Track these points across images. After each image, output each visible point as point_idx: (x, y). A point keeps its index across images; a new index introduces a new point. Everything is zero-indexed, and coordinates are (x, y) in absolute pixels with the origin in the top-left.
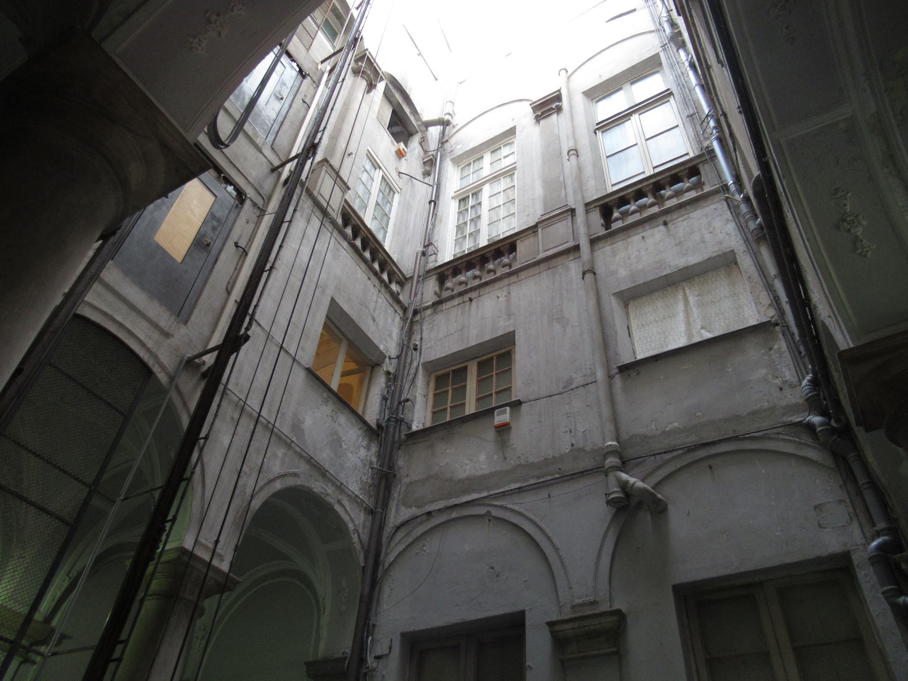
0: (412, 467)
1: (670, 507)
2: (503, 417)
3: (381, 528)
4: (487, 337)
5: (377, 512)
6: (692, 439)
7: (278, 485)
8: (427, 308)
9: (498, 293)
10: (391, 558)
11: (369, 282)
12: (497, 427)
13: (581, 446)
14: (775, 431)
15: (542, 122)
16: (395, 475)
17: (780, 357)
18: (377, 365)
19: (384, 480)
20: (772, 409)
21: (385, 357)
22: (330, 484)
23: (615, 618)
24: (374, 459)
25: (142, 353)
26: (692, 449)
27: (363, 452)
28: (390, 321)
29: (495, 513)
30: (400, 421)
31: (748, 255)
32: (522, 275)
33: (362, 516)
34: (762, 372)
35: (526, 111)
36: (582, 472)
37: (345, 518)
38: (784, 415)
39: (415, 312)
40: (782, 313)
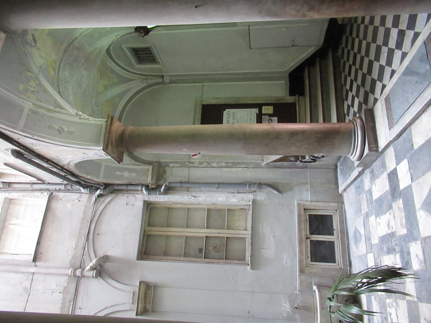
1: (107, 254)
6: (83, 238)
13: (63, 288)
14: (95, 208)
17: (66, 197)
20: (86, 206)
23: (142, 284)
26: (87, 240)
31: (12, 193)
34: (69, 205)
38: (90, 203)
40: (48, 190)
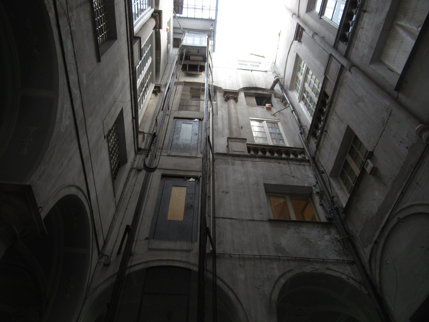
0: (356, 226)
2: (370, 165)
3: (363, 267)
4: (341, 139)
5: (356, 260)
7: (283, 281)
8: (316, 152)
9: (333, 117)
10: (378, 279)
11: (280, 165)
12: (371, 173)
15: (302, 40)
16: (353, 236)
18: (311, 193)
19: (348, 242)
21: (312, 187)
22: (315, 264)
24: (337, 236)
25: (182, 265)
27: (327, 237)
28: (303, 171)
29: (401, 216)
30: (337, 209)
32: (334, 100)
33: (348, 268)
35: (296, 42)
36: (422, 156)
37: (338, 274)
39: (313, 158)
